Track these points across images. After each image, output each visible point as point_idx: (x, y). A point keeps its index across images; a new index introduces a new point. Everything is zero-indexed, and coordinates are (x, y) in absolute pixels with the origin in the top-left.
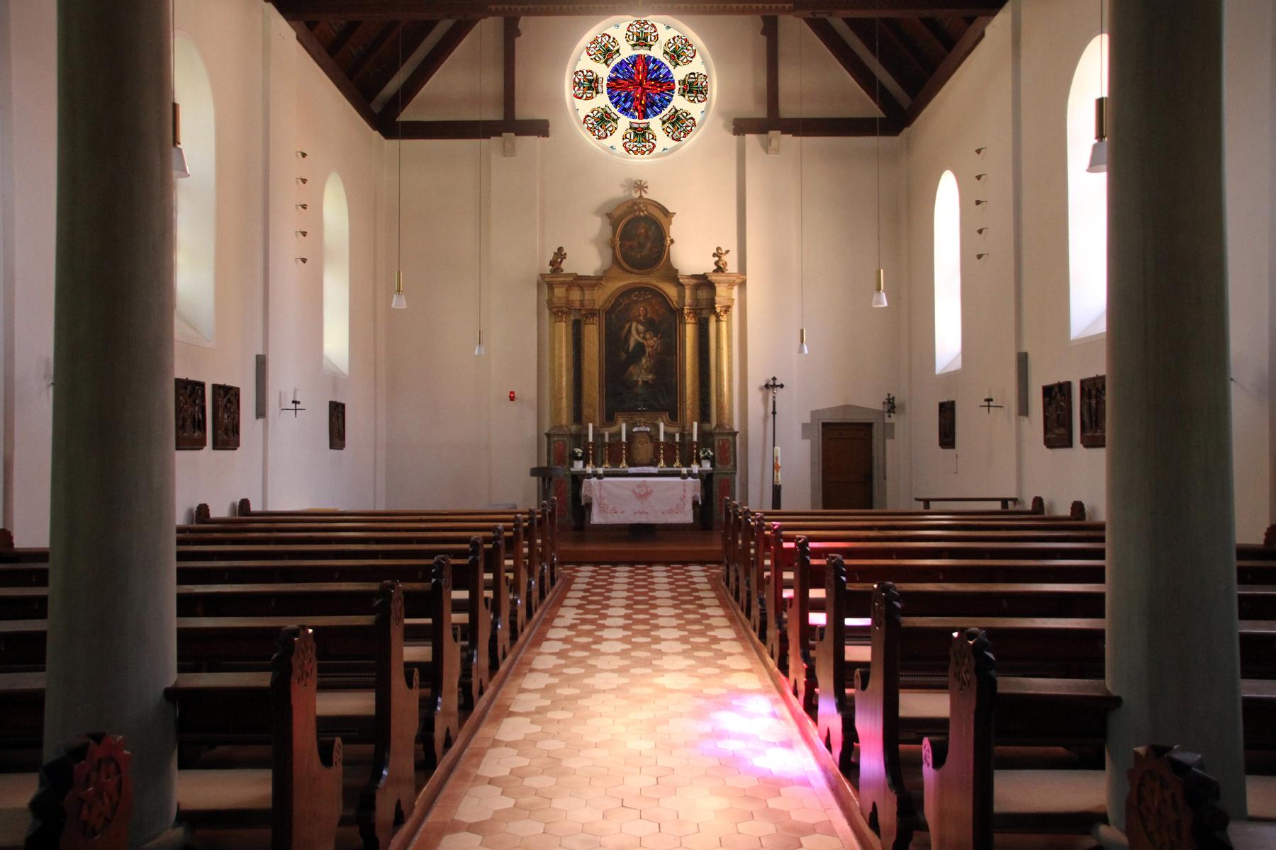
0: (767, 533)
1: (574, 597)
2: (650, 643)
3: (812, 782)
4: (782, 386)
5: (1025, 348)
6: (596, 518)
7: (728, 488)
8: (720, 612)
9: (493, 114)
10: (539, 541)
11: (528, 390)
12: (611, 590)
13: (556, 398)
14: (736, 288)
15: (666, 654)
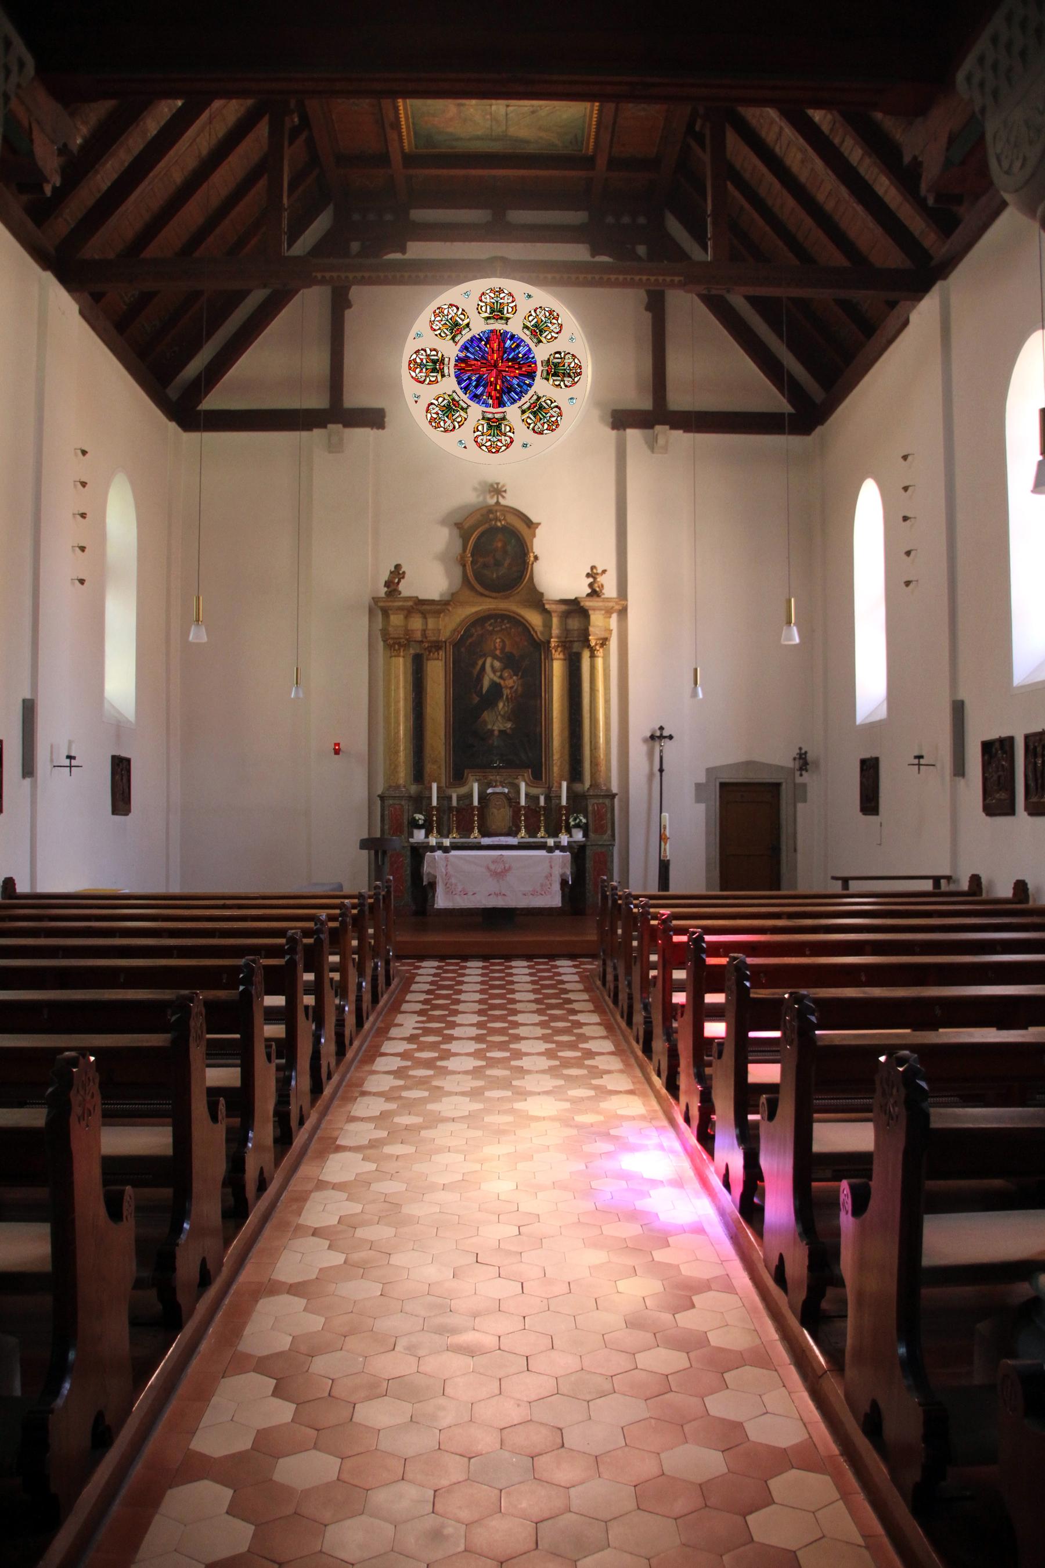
0: (653, 922)
1: (415, 999)
2: (508, 1059)
3: (708, 1229)
4: (671, 737)
5: (962, 695)
6: (442, 901)
7: (604, 862)
8: (595, 1018)
9: (316, 401)
10: (371, 931)
11: (357, 741)
12: (460, 992)
13: (391, 751)
14: (614, 616)
15: (529, 1072)
